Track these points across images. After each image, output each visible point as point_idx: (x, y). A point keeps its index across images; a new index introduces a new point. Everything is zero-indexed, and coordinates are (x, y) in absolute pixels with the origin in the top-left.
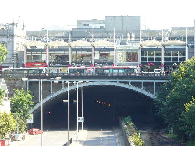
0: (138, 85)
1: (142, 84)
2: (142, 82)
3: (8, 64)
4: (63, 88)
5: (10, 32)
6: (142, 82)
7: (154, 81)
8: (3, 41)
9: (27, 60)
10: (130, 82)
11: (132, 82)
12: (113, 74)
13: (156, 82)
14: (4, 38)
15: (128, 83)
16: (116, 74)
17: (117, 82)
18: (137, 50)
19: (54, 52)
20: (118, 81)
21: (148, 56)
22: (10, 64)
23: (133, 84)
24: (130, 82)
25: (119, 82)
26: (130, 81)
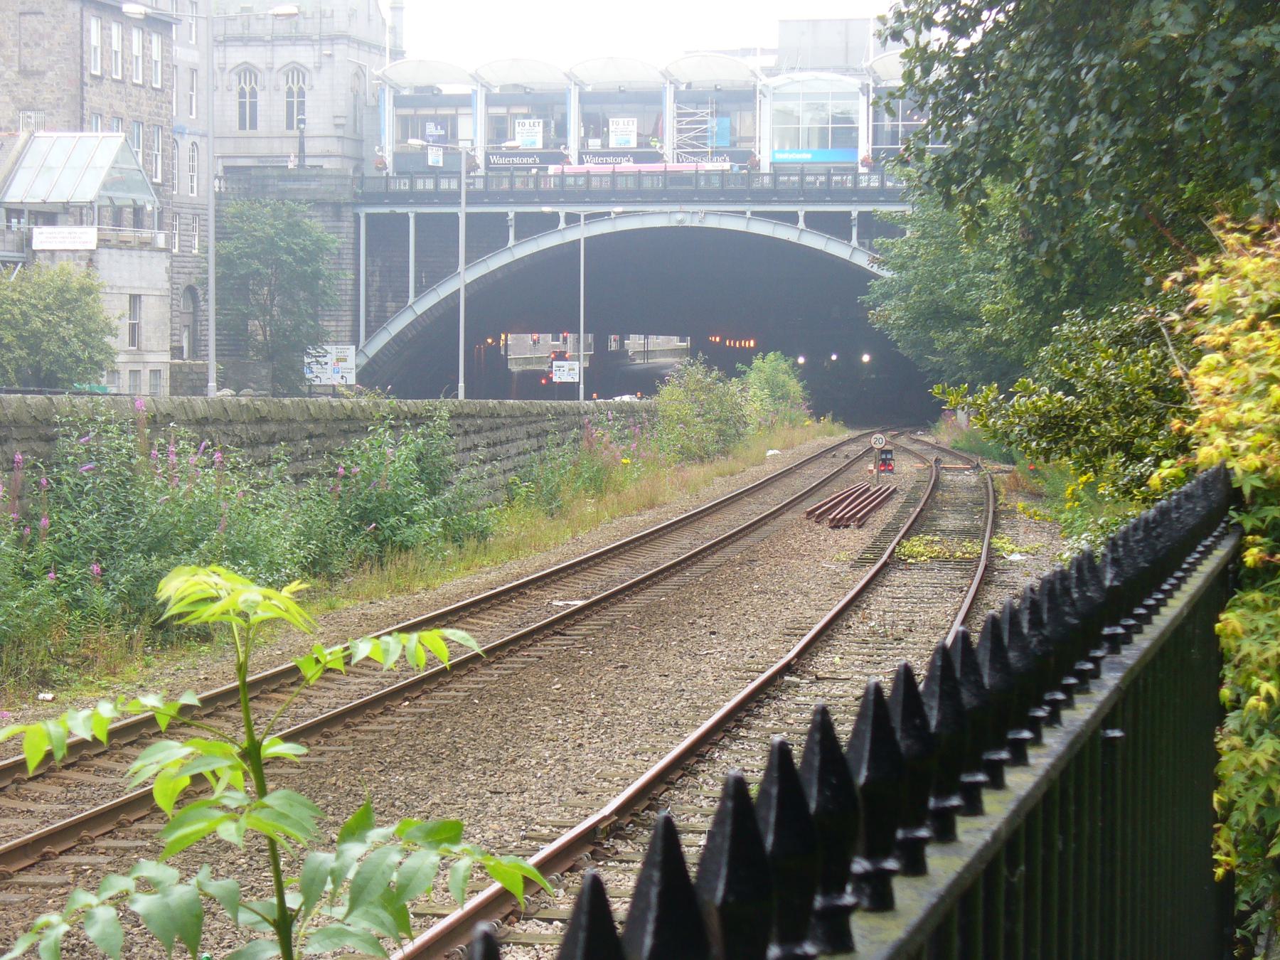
0: (835, 226)
1: (512, 223)
2: (855, 214)
3: (24, 147)
4: (511, 242)
5: (324, 20)
6: (855, 214)
7: (511, 211)
8: (297, 60)
9: (490, 141)
10: (801, 215)
11: (808, 216)
12: (570, 181)
13: (807, 214)
14: (298, 48)
15: (791, 218)
16: (581, 181)
17: (744, 213)
18: (853, 96)
19: (508, 106)
20: (749, 209)
21: (900, 123)
22: (325, 156)
23: (817, 222)
24: (801, 215)
25: (754, 213)
26: (801, 210)
